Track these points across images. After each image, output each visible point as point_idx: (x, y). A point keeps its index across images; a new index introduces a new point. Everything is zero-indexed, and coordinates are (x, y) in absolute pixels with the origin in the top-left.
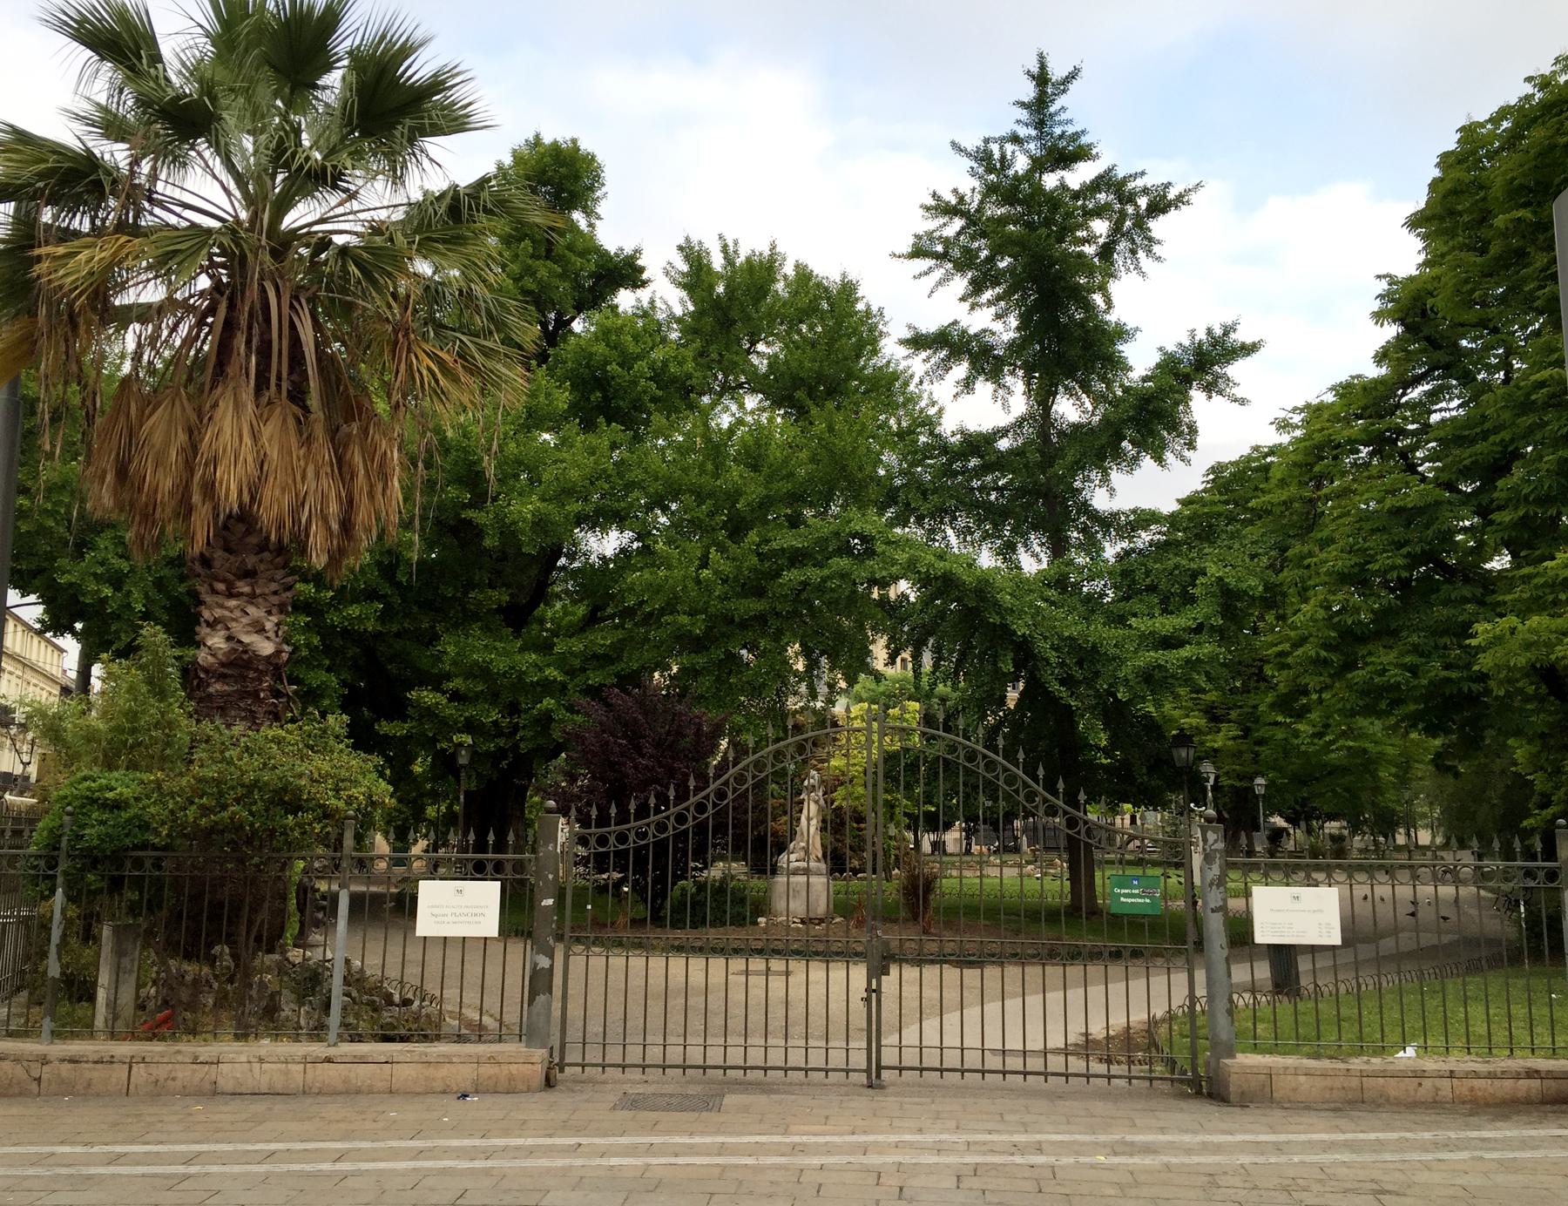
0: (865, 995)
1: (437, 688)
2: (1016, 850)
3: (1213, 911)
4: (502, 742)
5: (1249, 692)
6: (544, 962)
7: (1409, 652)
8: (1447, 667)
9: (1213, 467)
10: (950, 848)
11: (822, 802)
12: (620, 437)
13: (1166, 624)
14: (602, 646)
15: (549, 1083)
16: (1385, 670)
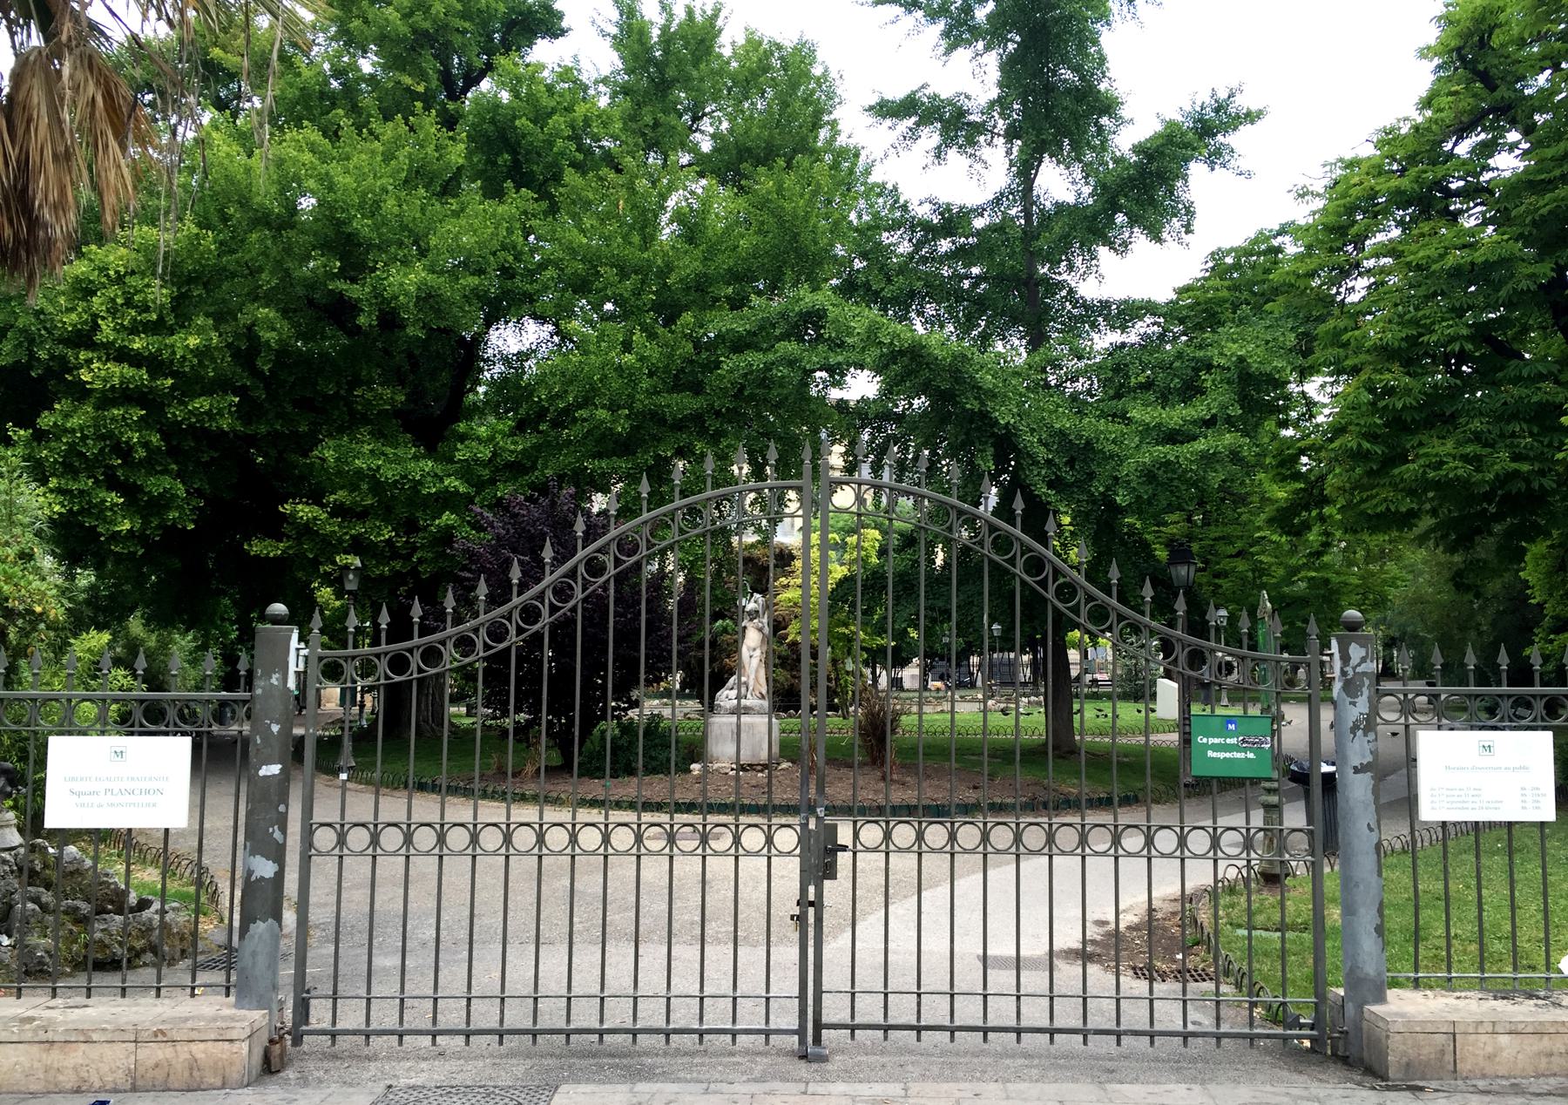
0: (797, 911)
1: (316, 499)
2: (973, 685)
3: (1356, 770)
4: (397, 565)
5: (1209, 524)
6: (265, 868)
7: (1469, 441)
8: (1516, 458)
9: (1213, 254)
10: (907, 685)
11: (766, 630)
12: (532, 207)
13: (1177, 415)
14: (512, 452)
15: (270, 1066)
16: (1442, 463)
